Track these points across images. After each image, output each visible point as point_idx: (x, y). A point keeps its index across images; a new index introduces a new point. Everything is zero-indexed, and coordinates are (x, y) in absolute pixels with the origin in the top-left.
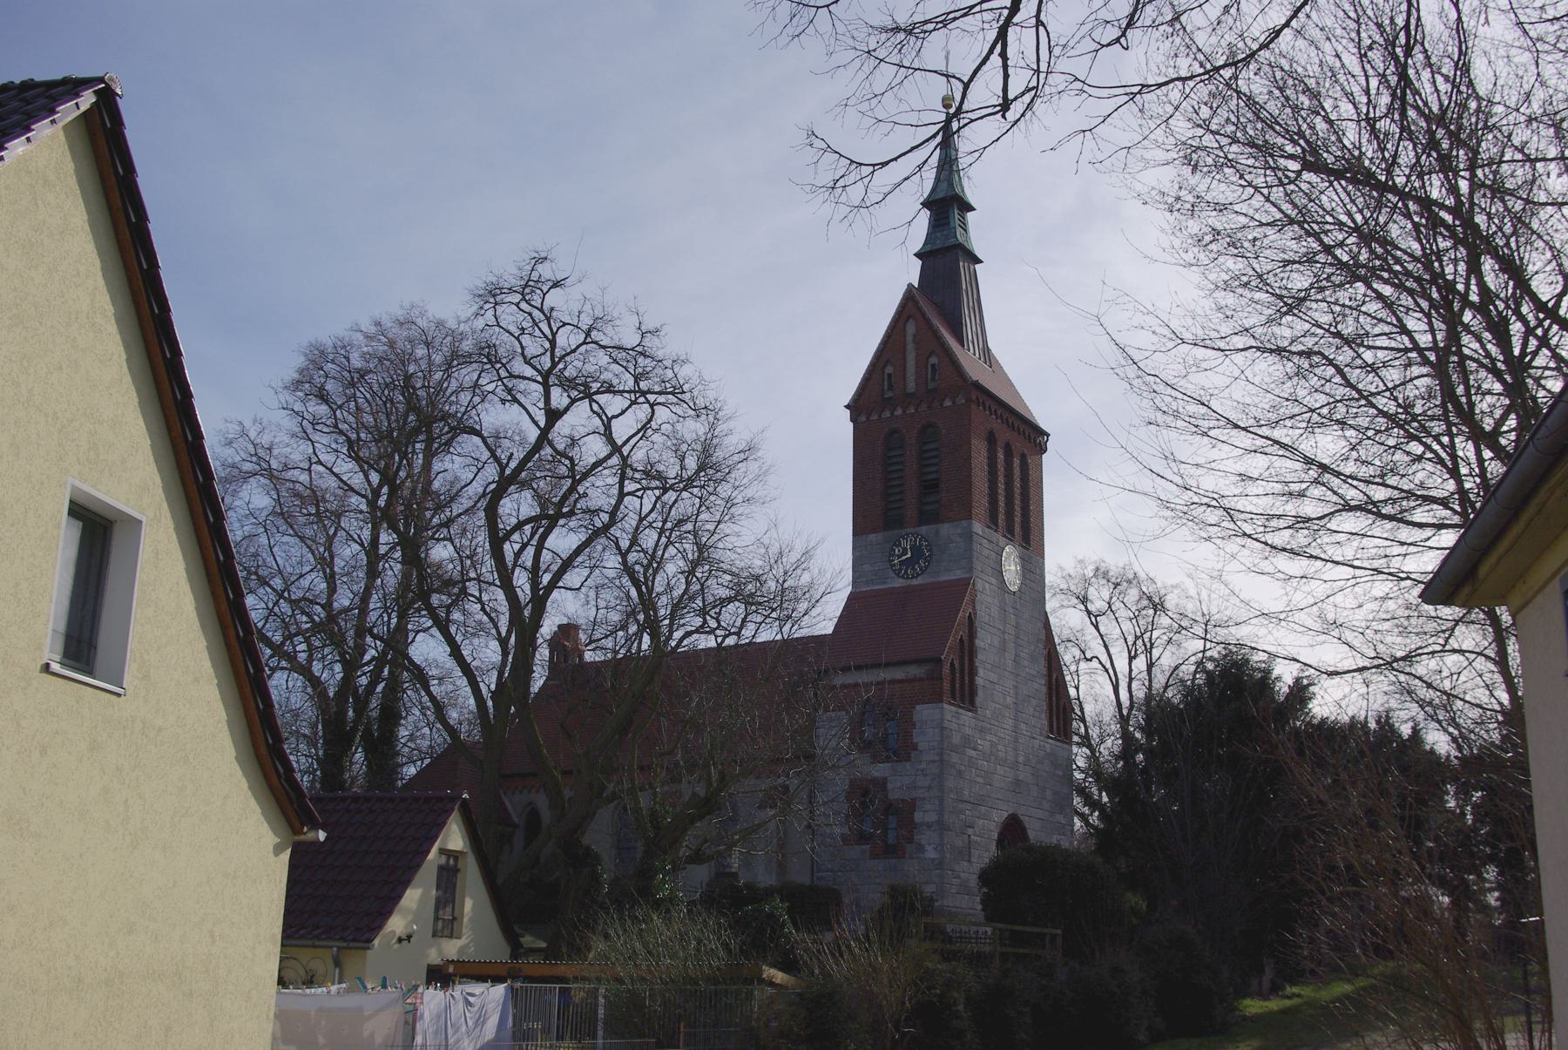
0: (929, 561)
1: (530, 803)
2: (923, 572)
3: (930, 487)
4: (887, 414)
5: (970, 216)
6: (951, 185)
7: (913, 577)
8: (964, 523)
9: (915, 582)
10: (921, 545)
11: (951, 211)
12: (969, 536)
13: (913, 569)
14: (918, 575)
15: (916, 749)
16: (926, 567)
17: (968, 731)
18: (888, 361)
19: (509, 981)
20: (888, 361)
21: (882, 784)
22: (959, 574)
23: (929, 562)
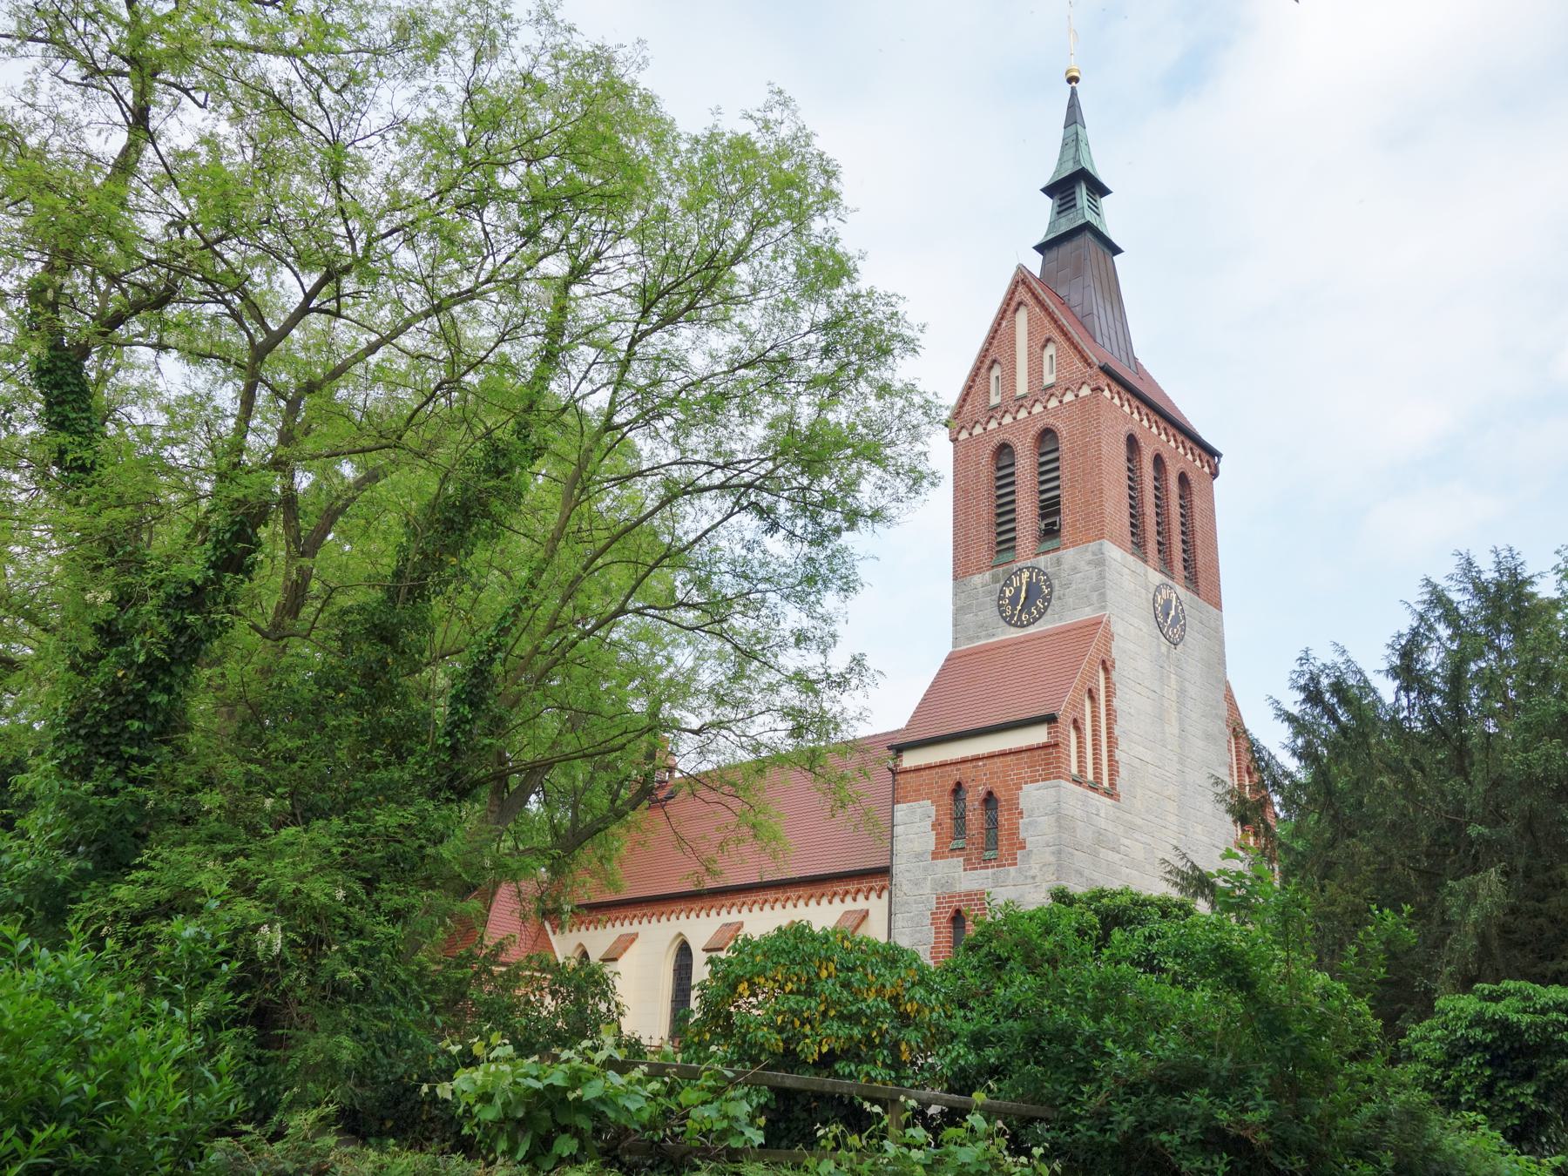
0: (1048, 600)
1: (680, 934)
2: (1041, 615)
3: (1050, 509)
4: (993, 425)
5: (1105, 202)
6: (1077, 161)
7: (1029, 624)
8: (1093, 546)
9: (1032, 630)
10: (1038, 581)
11: (1078, 190)
12: (1100, 562)
13: (1030, 613)
14: (1036, 620)
15: (1024, 848)
16: (1046, 608)
17: (1102, 823)
18: (994, 361)
19: (571, 1096)
20: (994, 361)
21: (978, 897)
22: (1086, 614)
23: (1049, 601)
